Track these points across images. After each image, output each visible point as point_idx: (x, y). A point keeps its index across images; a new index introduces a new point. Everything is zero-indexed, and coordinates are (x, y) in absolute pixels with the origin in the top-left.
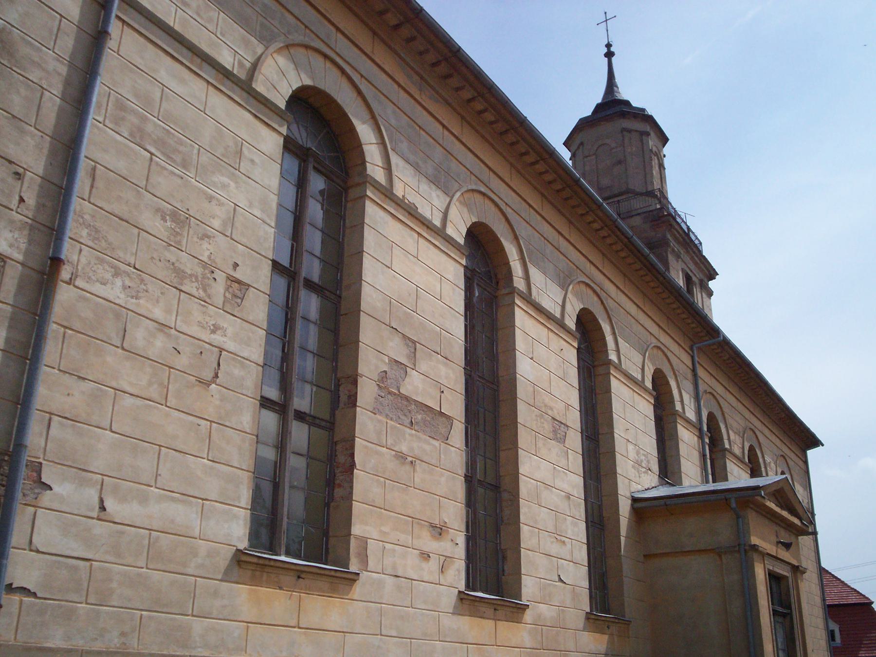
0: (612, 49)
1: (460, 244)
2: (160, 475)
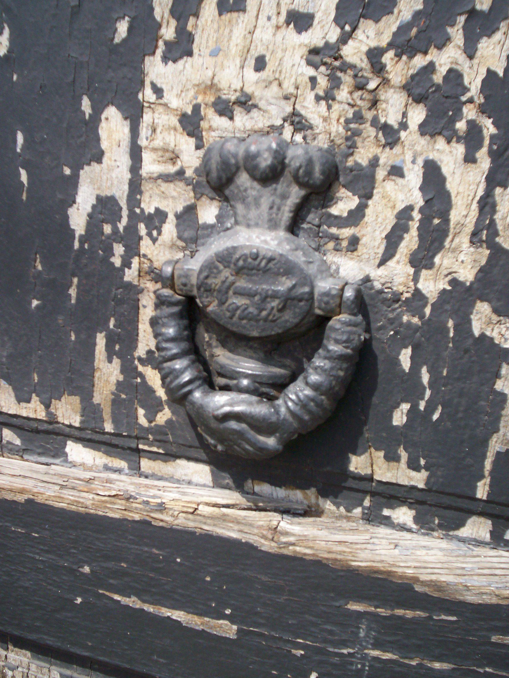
1: (391, 418)
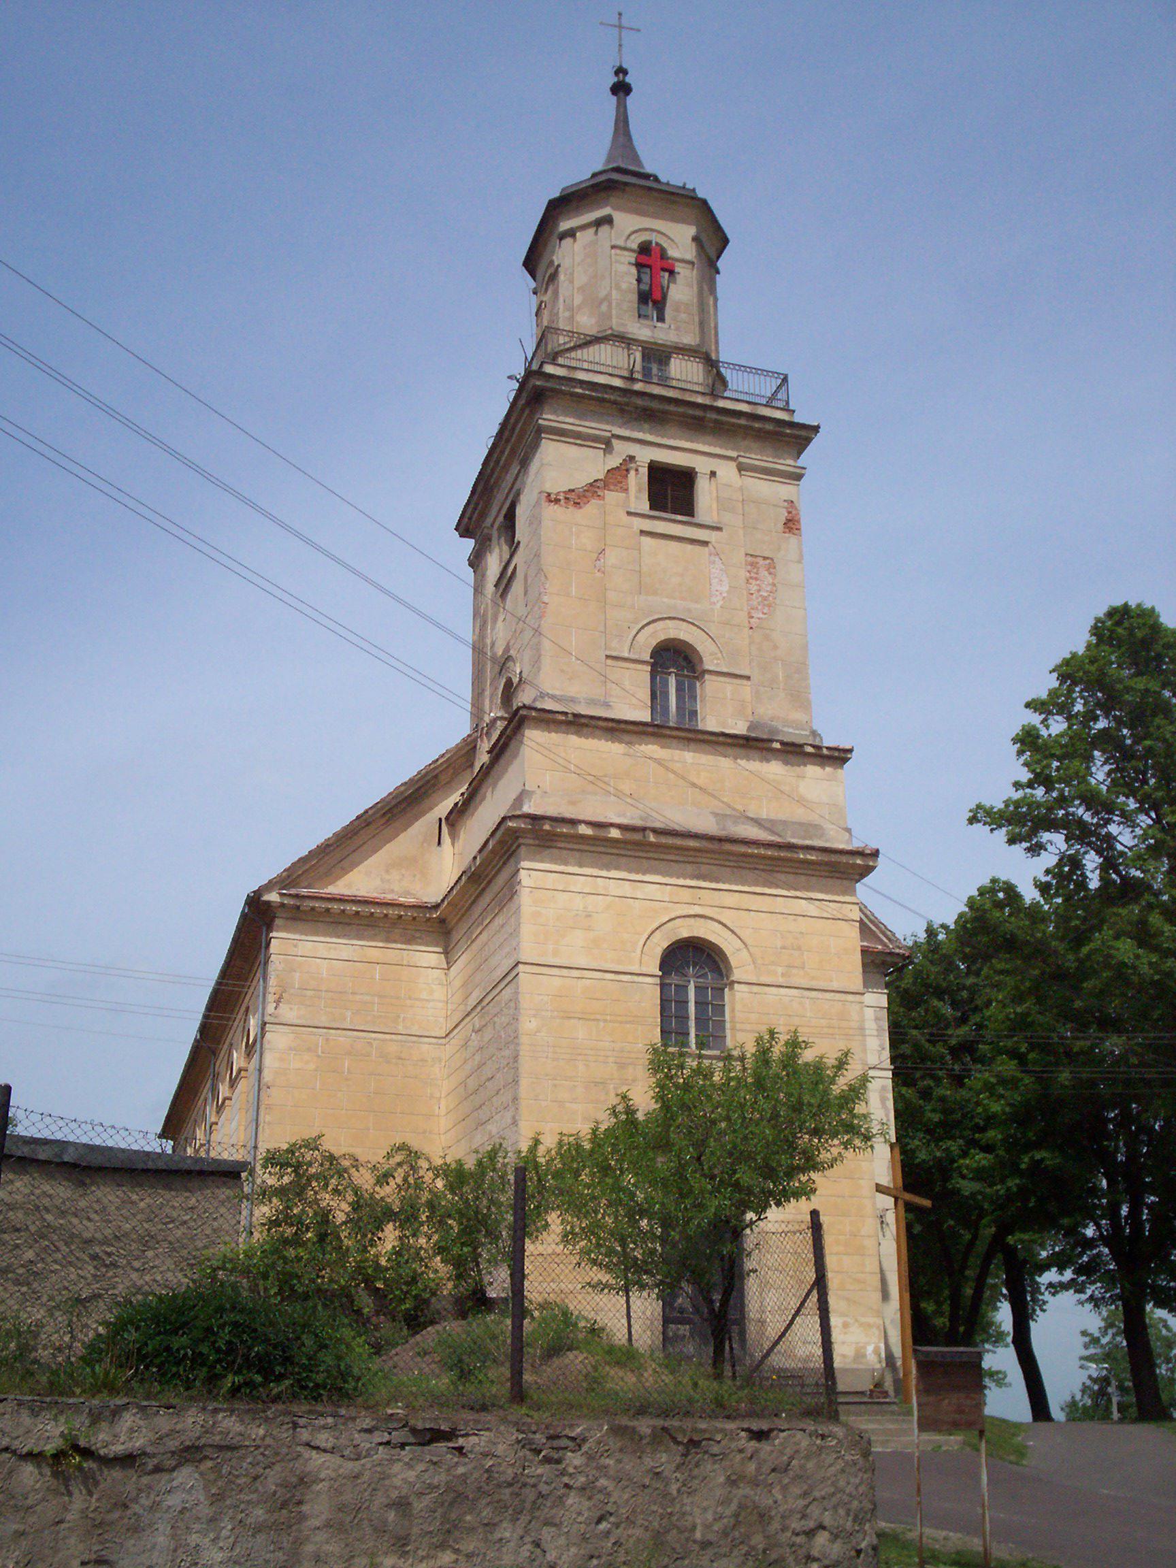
0: (628, 79)
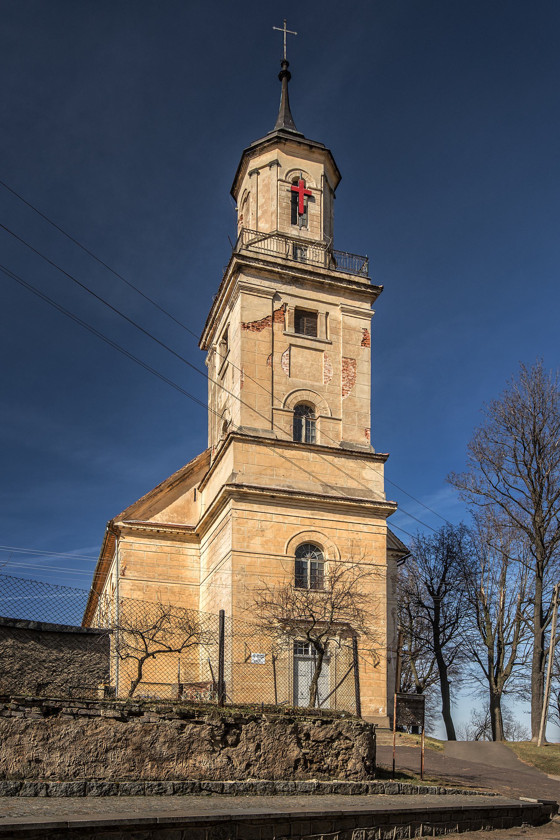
2: (154, 658)
